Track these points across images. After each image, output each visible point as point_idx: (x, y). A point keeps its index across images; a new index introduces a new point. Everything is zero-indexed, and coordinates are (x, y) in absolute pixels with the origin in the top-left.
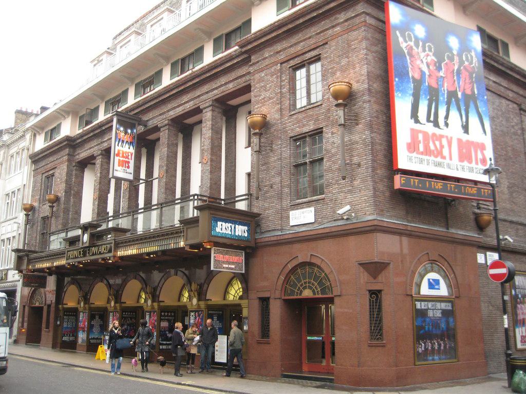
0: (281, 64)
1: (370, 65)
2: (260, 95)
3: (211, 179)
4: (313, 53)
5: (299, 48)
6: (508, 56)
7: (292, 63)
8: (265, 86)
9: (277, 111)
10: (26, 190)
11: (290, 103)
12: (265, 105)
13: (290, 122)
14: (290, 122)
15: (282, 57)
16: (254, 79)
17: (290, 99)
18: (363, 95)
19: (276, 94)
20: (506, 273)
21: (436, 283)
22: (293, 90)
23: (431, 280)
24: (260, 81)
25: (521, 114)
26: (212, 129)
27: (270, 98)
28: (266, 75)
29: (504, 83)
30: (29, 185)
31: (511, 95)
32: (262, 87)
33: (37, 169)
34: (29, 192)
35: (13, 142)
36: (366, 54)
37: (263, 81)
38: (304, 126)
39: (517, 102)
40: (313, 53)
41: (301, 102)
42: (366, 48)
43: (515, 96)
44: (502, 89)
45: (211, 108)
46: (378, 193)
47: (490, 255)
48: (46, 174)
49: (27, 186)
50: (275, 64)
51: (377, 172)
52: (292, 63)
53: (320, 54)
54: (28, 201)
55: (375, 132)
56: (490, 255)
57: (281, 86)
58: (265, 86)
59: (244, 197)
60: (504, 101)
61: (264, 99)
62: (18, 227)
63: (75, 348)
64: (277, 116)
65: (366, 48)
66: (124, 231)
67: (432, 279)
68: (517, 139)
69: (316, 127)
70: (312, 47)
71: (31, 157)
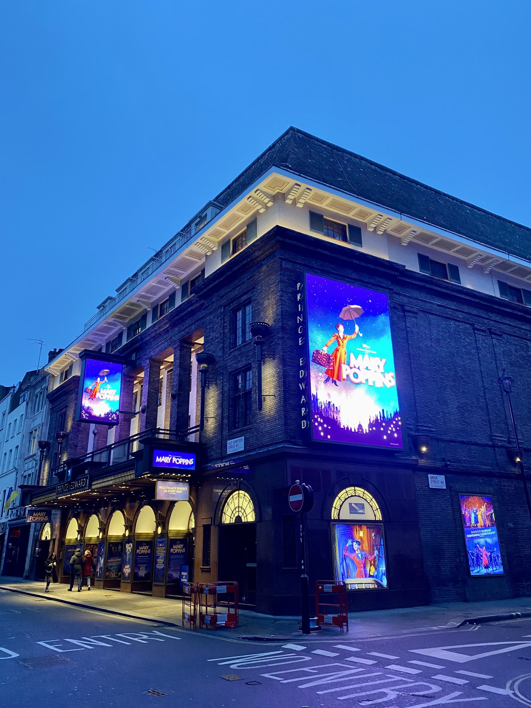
0: (225, 307)
1: (285, 305)
2: (209, 336)
3: (178, 412)
4: (245, 297)
5: (236, 292)
6: (458, 279)
7: (232, 306)
8: (213, 327)
9: (220, 349)
10: (44, 428)
11: (230, 342)
12: (213, 344)
13: (229, 359)
14: (229, 359)
15: (224, 301)
16: (206, 321)
17: (230, 338)
18: (278, 332)
19: (220, 334)
20: (301, 501)
21: (359, 507)
22: (234, 331)
23: (353, 505)
24: (211, 323)
25: (475, 333)
26: (180, 367)
27: (216, 338)
28: (214, 317)
29: (452, 305)
30: (47, 423)
31: (461, 316)
32: (211, 328)
33: (53, 408)
34: (46, 429)
35: (37, 384)
36: (281, 296)
37: (212, 323)
38: (239, 361)
39: (470, 322)
40: (245, 297)
41: (239, 342)
42: (281, 291)
43: (467, 316)
44: (450, 312)
45: (179, 348)
46: (290, 421)
47: (432, 478)
48: (60, 413)
49: (44, 425)
50: (220, 307)
51: (290, 402)
52: (232, 306)
53: (251, 297)
54: (45, 439)
55: (289, 366)
56: (432, 478)
57: (224, 327)
58: (213, 327)
59: (191, 431)
60: (452, 322)
61: (212, 339)
62: (36, 464)
63: (150, 589)
64: (220, 354)
65: (281, 291)
66: (100, 464)
67: (354, 504)
68: (470, 359)
69: (247, 362)
70: (245, 291)
71: (48, 396)
